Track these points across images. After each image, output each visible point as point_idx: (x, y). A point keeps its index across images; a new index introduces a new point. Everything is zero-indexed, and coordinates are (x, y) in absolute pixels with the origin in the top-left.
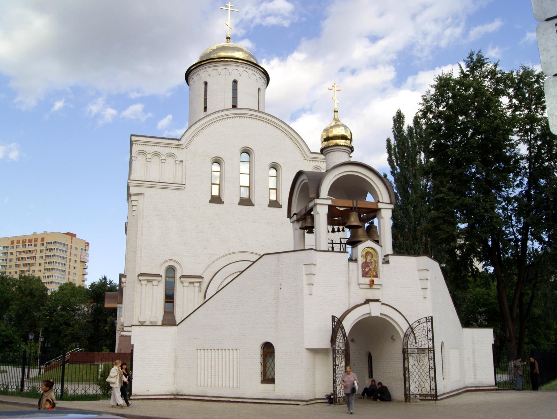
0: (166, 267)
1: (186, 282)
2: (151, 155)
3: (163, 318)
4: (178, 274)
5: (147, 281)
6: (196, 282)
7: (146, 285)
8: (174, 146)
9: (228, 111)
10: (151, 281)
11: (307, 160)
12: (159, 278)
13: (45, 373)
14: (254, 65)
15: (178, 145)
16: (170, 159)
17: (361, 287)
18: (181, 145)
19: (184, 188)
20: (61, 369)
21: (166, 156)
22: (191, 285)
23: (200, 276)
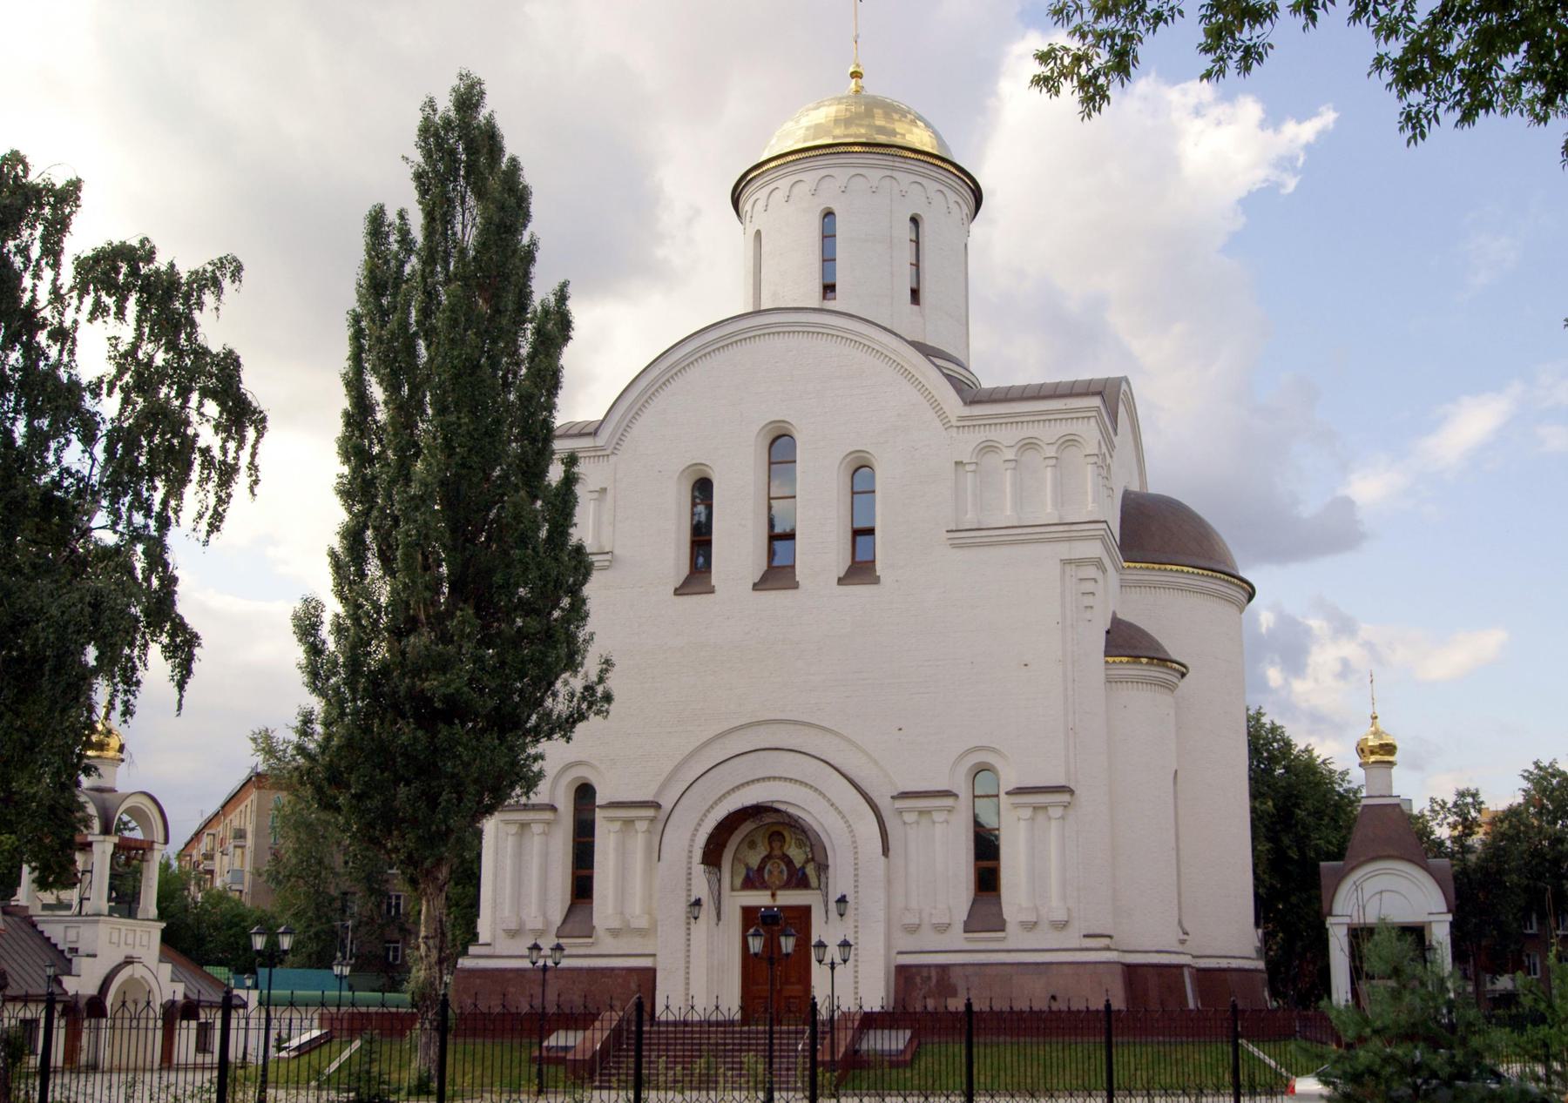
0: (973, 763)
1: (910, 810)
2: (1015, 449)
3: (969, 916)
4: (600, 799)
5: (1034, 808)
6: (1055, 805)
7: (917, 823)
8: (1028, 419)
9: (713, 332)
10: (1045, 808)
11: (958, 427)
12: (949, 802)
13: (1251, 1071)
14: (956, 172)
15: (596, 448)
16: (1030, 455)
17: (161, 839)
18: (602, 449)
19: (607, 563)
20: (1104, 1058)
21: (1056, 446)
22: (1041, 816)
23: (1063, 787)
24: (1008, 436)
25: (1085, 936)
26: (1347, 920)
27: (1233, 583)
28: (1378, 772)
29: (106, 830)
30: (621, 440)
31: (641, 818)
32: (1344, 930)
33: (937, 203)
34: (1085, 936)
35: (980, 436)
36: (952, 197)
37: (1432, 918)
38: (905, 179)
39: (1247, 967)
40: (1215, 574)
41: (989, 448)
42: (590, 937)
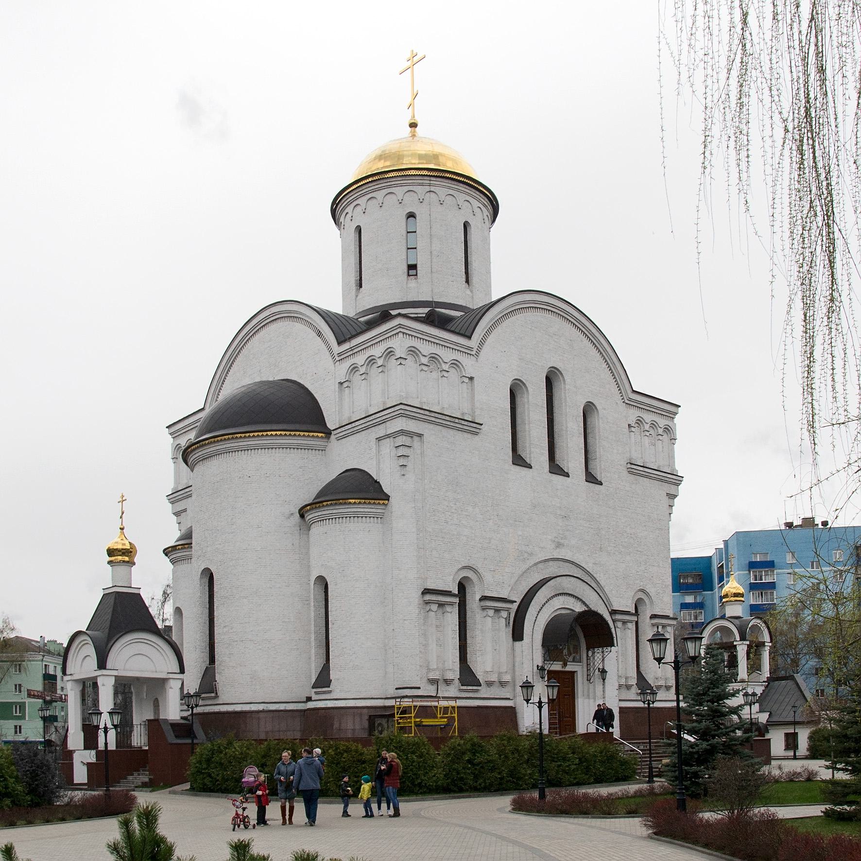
9: (264, 313)
24: (360, 359)
25: (396, 689)
26: (115, 673)
27: (205, 445)
28: (122, 569)
29: (743, 638)
30: (621, 396)
31: (670, 625)
32: (112, 681)
33: (475, 211)
34: (396, 689)
35: (347, 364)
36: (476, 204)
37: (171, 676)
38: (461, 197)
39: (299, 708)
40: (216, 439)
41: (354, 369)
42: (329, 687)
